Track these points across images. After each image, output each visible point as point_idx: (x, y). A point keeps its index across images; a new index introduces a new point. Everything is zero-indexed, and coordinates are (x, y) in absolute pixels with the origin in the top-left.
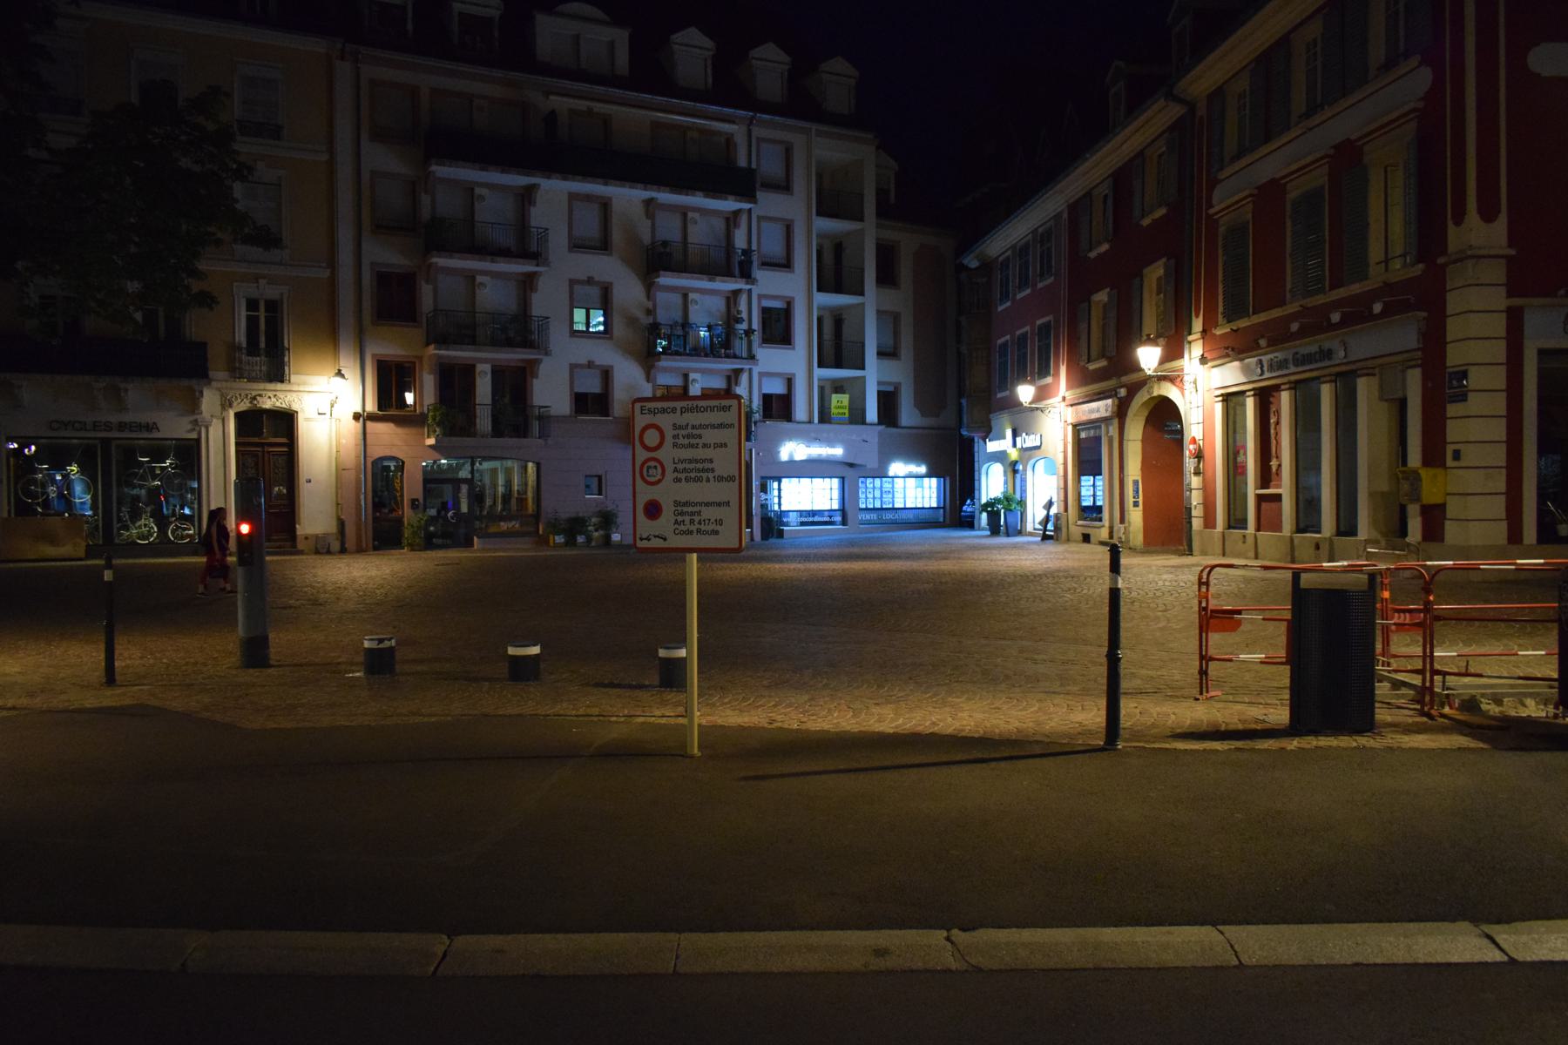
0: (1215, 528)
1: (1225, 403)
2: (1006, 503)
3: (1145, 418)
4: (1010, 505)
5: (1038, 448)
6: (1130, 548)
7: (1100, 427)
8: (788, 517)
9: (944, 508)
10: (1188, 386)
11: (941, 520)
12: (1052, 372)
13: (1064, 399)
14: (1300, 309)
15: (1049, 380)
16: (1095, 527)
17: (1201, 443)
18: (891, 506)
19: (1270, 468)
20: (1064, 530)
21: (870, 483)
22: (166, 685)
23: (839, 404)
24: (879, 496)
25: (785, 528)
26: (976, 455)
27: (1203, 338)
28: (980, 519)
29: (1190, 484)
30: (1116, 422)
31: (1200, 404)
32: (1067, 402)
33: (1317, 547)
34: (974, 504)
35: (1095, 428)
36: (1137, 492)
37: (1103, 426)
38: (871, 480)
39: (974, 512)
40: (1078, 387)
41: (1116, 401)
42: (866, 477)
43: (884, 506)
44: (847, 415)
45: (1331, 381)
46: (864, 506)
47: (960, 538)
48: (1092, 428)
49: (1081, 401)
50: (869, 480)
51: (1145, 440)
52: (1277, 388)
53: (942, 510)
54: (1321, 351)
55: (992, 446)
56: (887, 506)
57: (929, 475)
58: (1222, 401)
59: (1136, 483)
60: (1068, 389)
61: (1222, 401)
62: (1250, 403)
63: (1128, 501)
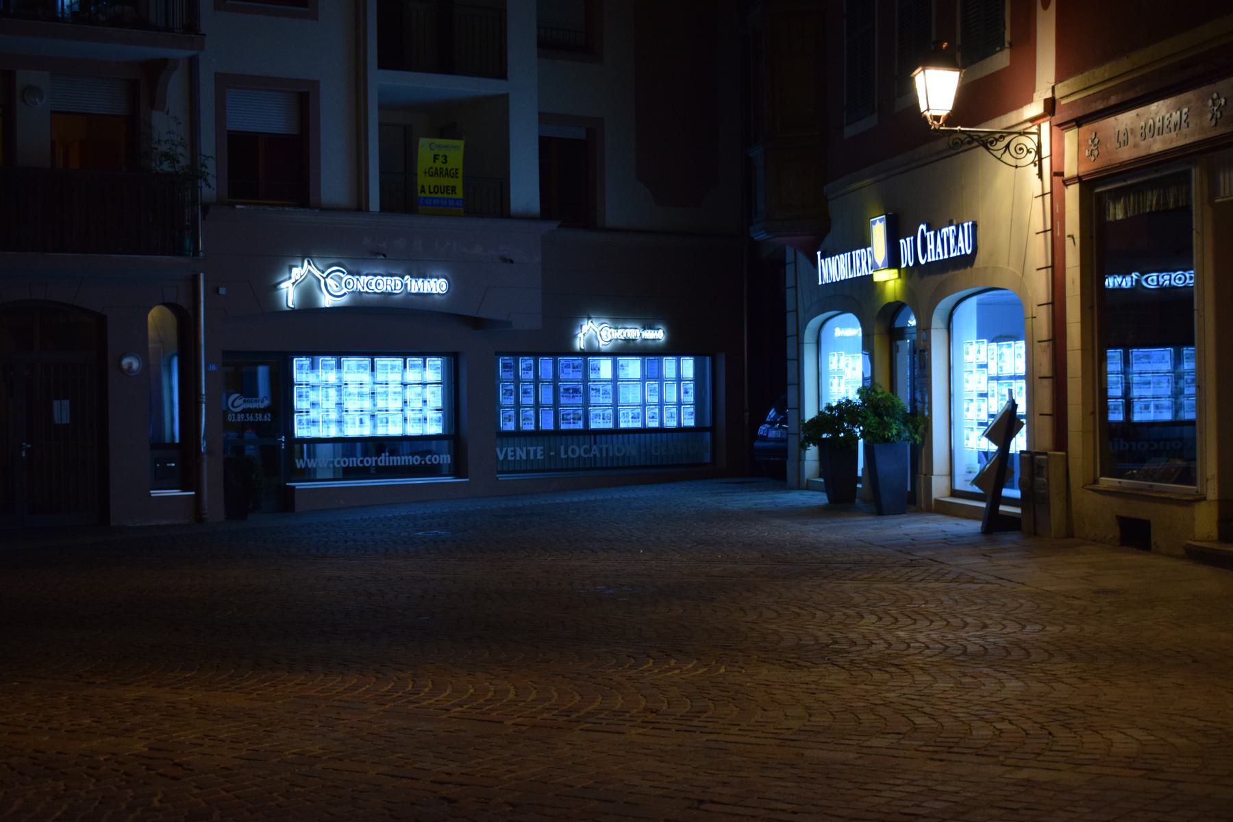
2: (873, 420)
4: (886, 426)
5: (966, 261)
7: (1185, 178)
8: (312, 455)
9: (713, 429)
11: (707, 458)
12: (1007, 37)
13: (1051, 106)
15: (1001, 60)
16: (1169, 501)
18: (580, 425)
20: (1057, 505)
21: (529, 369)
23: (439, 164)
24: (550, 401)
25: (299, 485)
26: (790, 294)
28: (801, 459)
32: (1059, 117)
34: (784, 421)
37: (1195, 173)
38: (530, 361)
39: (785, 440)
40: (1097, 62)
42: (516, 354)
43: (563, 426)
44: (459, 194)
46: (510, 426)
47: (759, 515)
48: (1151, 185)
49: (1113, 100)
50: (525, 362)
53: (708, 435)
55: (833, 269)
56: (572, 427)
57: (674, 348)
60: (1060, 78)
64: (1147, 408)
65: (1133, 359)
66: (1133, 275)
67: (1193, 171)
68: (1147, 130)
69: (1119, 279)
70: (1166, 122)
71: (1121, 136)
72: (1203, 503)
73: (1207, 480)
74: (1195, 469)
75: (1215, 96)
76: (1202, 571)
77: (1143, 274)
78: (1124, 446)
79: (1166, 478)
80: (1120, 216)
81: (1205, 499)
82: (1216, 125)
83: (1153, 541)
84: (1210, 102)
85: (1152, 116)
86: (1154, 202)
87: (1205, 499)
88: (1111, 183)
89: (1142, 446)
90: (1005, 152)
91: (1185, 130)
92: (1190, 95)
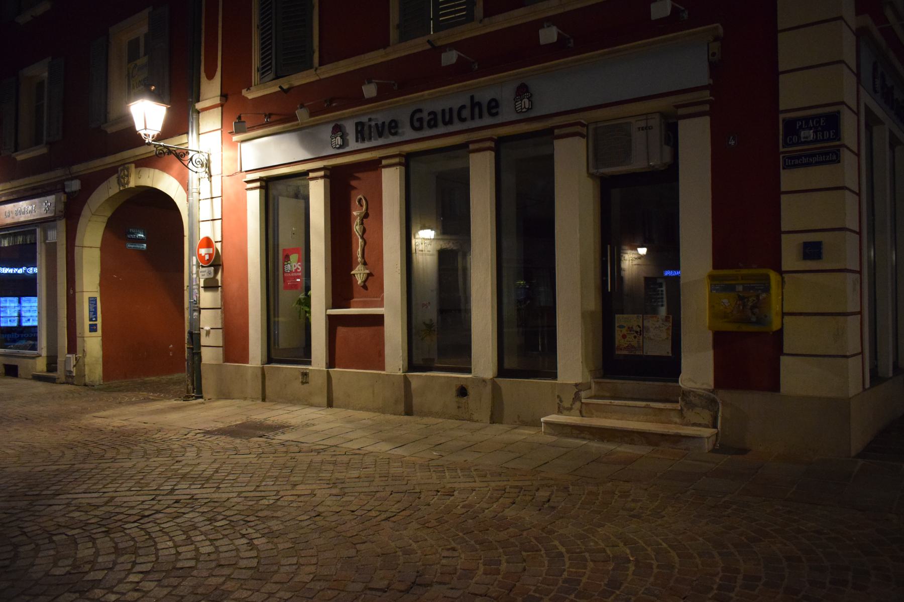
0: (247, 362)
1: (263, 191)
3: (106, 219)
6: (85, 385)
7: (34, 232)
10: (195, 175)
14: (428, 47)
17: (218, 246)
19: (350, 278)
22: (504, 519)
27: (222, 105)
29: (197, 302)
30: (62, 224)
31: (217, 192)
33: (462, 392)
35: (24, 234)
36: (95, 313)
37: (38, 230)
41: (63, 198)
45: (399, 164)
51: (104, 248)
52: (375, 166)
54: (475, 104)
58: (260, 187)
59: (93, 301)
61: (260, 187)
62: (317, 192)
63: (83, 323)
64: (29, 320)
65: (22, 302)
66: (23, 268)
67: (37, 229)
68: (18, 212)
69: (16, 270)
70: (26, 210)
71: (7, 213)
72: (40, 358)
73: (42, 349)
74: (37, 345)
75: (46, 202)
76: (39, 384)
77: (28, 268)
78: (17, 336)
79: (25, 348)
80: (6, 245)
81: (41, 356)
82: (46, 213)
83: (19, 374)
84: (44, 204)
85: (20, 206)
86: (21, 240)
87: (41, 356)
88: (16, 229)
89: (26, 335)
90: (189, 162)
91: (34, 214)
92: (36, 200)
